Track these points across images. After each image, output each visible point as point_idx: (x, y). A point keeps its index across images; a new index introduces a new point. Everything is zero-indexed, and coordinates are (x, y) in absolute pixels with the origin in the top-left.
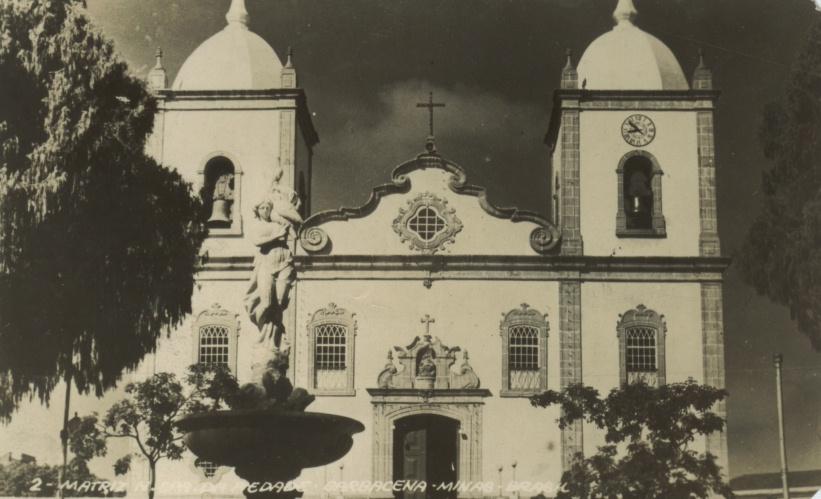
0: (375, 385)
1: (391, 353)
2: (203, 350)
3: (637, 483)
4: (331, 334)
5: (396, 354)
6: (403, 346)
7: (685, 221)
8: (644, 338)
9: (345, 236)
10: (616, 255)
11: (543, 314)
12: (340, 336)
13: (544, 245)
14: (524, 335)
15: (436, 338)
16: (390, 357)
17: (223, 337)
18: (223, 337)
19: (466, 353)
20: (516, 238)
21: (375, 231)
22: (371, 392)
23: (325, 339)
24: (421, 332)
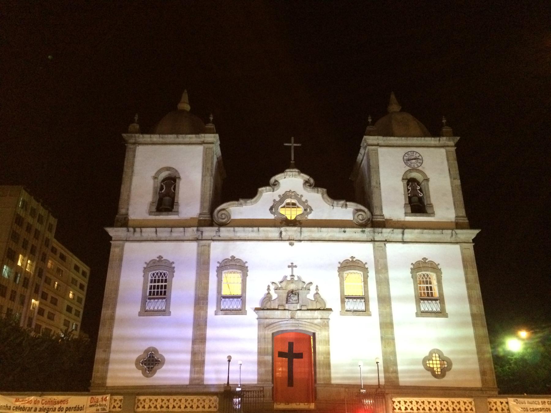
0: (258, 306)
1: (269, 286)
2: (165, 294)
3: (19, 264)
4: (159, 277)
5: (272, 287)
6: (277, 281)
7: (445, 204)
8: (157, 278)
9: (239, 210)
10: (392, 229)
11: (364, 263)
12: (161, 278)
13: (362, 220)
14: (162, 277)
15: (298, 277)
16: (269, 289)
17: (164, 278)
18: (428, 280)
19: (317, 286)
20: (345, 212)
21: (258, 207)
22: (257, 309)
23: (155, 280)
24: (288, 272)
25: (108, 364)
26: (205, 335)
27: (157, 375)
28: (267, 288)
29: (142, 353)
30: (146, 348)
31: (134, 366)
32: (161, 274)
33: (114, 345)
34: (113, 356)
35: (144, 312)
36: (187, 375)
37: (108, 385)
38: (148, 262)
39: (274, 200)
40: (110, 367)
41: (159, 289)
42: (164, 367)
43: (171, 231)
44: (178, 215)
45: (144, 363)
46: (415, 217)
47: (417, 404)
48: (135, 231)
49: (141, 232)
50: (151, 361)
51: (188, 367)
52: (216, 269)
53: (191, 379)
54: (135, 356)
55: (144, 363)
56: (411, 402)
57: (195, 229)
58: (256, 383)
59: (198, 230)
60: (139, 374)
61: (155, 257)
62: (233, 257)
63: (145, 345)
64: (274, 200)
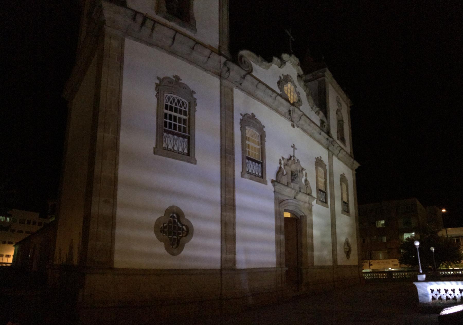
25: (113, 227)
26: (234, 200)
27: (187, 251)
28: (279, 161)
29: (163, 215)
30: (167, 206)
31: (152, 235)
32: (179, 101)
33: (122, 194)
34: (120, 213)
35: (160, 150)
36: (217, 255)
37: (116, 265)
38: (162, 77)
39: (156, 84)
40: (118, 231)
41: (176, 124)
42: (194, 240)
43: (193, 48)
44: (194, 34)
45: (163, 230)
46: (348, 133)
47: (446, 292)
48: (143, 24)
49: (153, 29)
50: (175, 229)
51: (218, 243)
52: (239, 121)
53: (222, 260)
54: (153, 218)
55: (163, 230)
56: (453, 291)
57: (223, 60)
58: (274, 266)
59: (225, 64)
60: (161, 249)
61: (170, 74)
62: (253, 115)
63: (168, 202)
64: (156, 84)
